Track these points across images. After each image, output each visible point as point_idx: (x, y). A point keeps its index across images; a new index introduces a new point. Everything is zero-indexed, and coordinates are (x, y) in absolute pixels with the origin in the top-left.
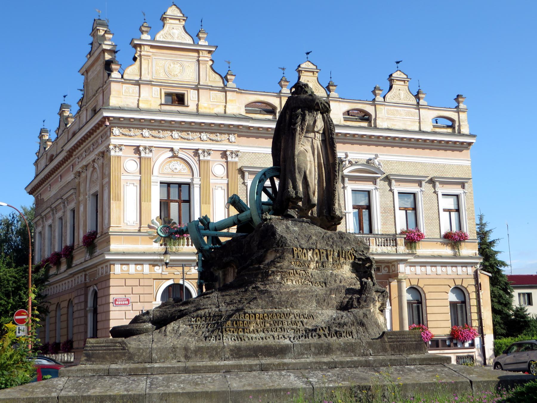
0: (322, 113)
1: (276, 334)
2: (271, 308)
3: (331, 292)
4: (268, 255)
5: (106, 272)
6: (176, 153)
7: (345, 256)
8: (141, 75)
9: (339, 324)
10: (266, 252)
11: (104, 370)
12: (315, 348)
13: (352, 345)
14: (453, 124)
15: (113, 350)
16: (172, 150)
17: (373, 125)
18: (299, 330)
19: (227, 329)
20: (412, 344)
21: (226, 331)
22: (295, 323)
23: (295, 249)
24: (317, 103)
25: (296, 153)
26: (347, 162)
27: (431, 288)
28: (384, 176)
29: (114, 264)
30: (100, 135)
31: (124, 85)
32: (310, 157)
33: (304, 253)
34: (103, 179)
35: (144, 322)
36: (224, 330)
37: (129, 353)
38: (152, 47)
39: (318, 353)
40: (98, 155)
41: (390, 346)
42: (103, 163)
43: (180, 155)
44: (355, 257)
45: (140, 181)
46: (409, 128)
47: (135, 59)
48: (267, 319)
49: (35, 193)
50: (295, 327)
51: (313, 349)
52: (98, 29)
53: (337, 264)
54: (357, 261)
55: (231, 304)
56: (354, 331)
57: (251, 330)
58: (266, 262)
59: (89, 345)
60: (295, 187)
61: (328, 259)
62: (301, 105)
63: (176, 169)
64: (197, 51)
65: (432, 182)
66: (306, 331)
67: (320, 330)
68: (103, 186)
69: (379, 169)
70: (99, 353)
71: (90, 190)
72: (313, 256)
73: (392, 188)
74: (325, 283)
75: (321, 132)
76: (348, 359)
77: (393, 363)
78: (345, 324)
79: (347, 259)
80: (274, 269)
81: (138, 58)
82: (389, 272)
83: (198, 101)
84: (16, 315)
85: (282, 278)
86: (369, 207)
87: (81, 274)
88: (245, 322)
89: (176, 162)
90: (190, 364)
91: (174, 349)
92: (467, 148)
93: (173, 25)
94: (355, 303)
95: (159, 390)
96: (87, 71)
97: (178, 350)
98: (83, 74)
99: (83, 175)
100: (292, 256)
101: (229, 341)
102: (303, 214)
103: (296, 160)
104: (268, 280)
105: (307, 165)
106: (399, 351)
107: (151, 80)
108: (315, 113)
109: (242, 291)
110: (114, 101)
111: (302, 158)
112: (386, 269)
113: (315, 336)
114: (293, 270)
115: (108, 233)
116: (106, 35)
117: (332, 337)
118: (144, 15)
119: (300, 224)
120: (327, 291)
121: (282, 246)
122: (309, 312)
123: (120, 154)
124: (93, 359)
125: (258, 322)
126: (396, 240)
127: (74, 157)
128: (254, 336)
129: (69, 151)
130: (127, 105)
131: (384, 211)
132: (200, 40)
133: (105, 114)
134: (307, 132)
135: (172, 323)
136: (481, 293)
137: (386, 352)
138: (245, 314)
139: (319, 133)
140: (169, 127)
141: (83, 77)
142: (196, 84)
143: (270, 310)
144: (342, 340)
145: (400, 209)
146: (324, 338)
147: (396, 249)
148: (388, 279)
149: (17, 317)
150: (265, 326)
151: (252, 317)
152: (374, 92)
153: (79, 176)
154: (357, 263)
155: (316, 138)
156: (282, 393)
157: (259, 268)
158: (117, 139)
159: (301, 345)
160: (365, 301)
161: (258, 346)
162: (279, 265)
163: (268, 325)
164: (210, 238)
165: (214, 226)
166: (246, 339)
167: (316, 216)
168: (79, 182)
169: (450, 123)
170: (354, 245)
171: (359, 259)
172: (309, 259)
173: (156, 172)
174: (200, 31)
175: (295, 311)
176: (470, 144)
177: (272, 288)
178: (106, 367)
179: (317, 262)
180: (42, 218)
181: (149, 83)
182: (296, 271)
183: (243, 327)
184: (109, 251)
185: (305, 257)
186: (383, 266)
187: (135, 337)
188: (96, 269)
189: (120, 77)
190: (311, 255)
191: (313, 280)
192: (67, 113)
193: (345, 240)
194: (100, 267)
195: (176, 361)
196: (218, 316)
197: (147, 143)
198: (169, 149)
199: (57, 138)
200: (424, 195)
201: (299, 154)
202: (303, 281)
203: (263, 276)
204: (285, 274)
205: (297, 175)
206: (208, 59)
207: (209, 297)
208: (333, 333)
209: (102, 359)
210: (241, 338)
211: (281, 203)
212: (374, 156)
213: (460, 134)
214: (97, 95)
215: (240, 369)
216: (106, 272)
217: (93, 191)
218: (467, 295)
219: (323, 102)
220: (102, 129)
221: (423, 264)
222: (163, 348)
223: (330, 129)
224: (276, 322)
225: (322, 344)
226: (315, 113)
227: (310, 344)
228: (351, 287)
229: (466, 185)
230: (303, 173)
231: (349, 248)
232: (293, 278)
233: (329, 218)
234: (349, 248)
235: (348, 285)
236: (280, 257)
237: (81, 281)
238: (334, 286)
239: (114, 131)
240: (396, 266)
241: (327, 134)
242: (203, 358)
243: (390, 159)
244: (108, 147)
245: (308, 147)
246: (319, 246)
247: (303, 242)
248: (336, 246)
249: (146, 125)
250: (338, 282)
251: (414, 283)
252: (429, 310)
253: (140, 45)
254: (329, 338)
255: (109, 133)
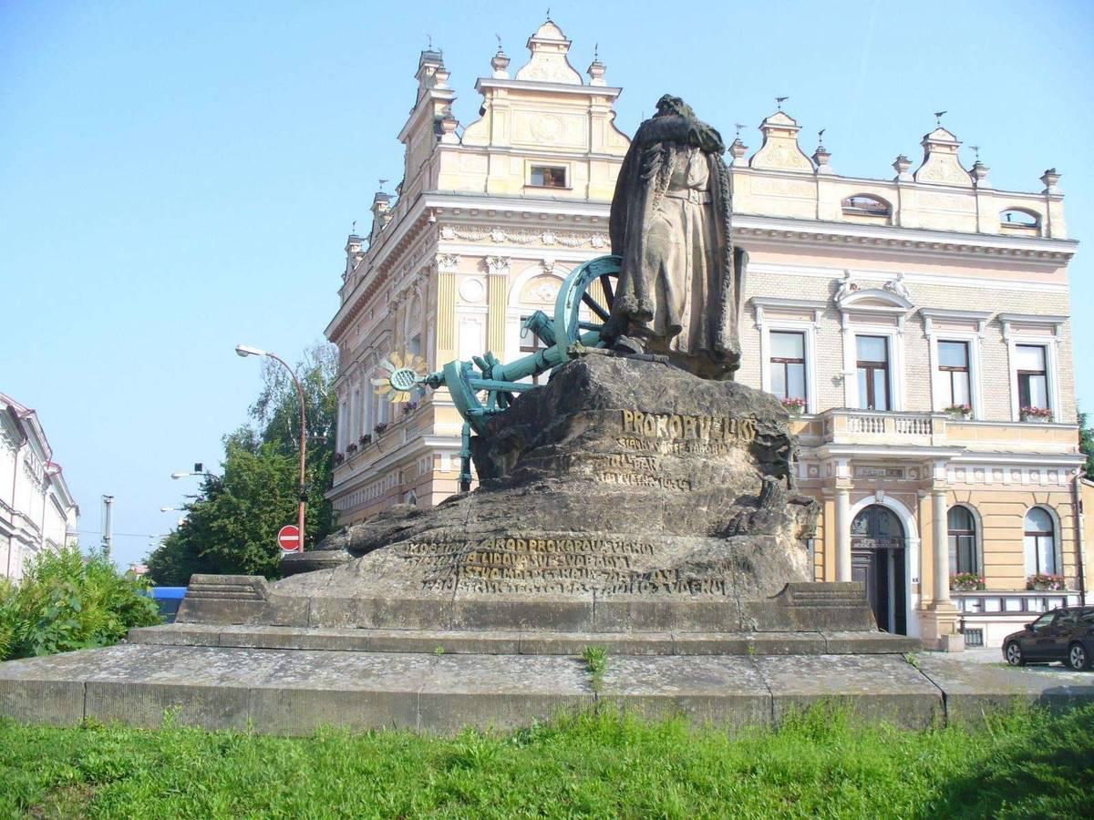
0: (706, 153)
1: (568, 581)
2: (563, 530)
3: (698, 500)
4: (574, 424)
5: (428, 469)
6: (549, 268)
7: (736, 430)
8: (491, 138)
9: (698, 565)
10: (570, 418)
11: (211, 635)
12: (639, 612)
13: (716, 607)
14: (1037, 222)
15: (239, 598)
16: (542, 262)
17: (894, 223)
18: (618, 574)
19: (468, 568)
20: (842, 611)
21: (465, 571)
22: (612, 561)
23: (627, 412)
24: (693, 131)
25: (647, 225)
26: (848, 286)
27: (993, 508)
28: (914, 310)
29: (440, 457)
30: (423, 240)
31: (463, 155)
32: (676, 235)
33: (649, 422)
34: (427, 313)
35: (336, 549)
36: (461, 569)
37: (268, 606)
38: (511, 91)
39: (644, 624)
40: (420, 273)
41: (798, 613)
42: (428, 287)
43: (555, 272)
44: (757, 431)
45: (487, 314)
46: (959, 229)
47: (482, 112)
48: (553, 550)
49: (339, 339)
50: (610, 568)
51: (634, 615)
52: (426, 67)
53: (718, 443)
54: (760, 441)
55: (488, 519)
56: (729, 581)
57: (517, 572)
58: (570, 438)
59: (196, 586)
60: (638, 293)
61: (699, 435)
62: (667, 136)
63: (549, 295)
64: (589, 97)
65: (999, 322)
66: (631, 577)
67: (656, 575)
68: (427, 323)
69: (903, 298)
70: (212, 602)
71: (409, 332)
72: (668, 429)
73: (927, 332)
74: (689, 483)
75: (704, 187)
76: (703, 638)
77: (795, 649)
78: (710, 565)
79: (740, 436)
80: (581, 452)
81: (488, 112)
82: (918, 479)
83: (589, 180)
84: (282, 535)
85: (595, 471)
86: (885, 366)
87: (393, 472)
88: (505, 555)
89: (548, 284)
90: (379, 633)
91: (353, 603)
92: (1063, 263)
93: (546, 54)
94: (745, 524)
95: (289, 683)
96: (410, 137)
97: (361, 605)
98: (403, 142)
99: (401, 307)
100: (620, 428)
101: (468, 592)
102: (657, 344)
103: (644, 241)
104: (568, 474)
105: (667, 250)
106: (816, 625)
107: (509, 146)
108: (690, 151)
109: (517, 496)
110: (445, 182)
111: (656, 236)
112: (913, 473)
113: (646, 587)
114: (620, 454)
115: (431, 402)
116: (438, 76)
117: (680, 591)
118: (499, 39)
119: (645, 364)
120: (689, 499)
121: (600, 408)
122: (646, 539)
123: (453, 269)
124: (200, 614)
125: (535, 557)
126: (930, 422)
127: (390, 278)
128: (523, 583)
129: (381, 268)
130: (468, 188)
131: (913, 372)
132: (593, 78)
133: (429, 204)
134: (673, 186)
135: (373, 552)
136: (1081, 519)
137: (787, 625)
138: (506, 539)
139: (699, 191)
140: (538, 224)
141: (405, 145)
142: (586, 151)
143: (560, 533)
144: (698, 598)
145: (940, 370)
146: (665, 592)
147: (931, 439)
148: (916, 491)
149: (283, 538)
150: (547, 564)
151: (521, 544)
152: (896, 165)
153: (396, 309)
154: (761, 445)
155: (691, 199)
156: (528, 704)
157: (553, 451)
158: (450, 244)
159: (611, 605)
160: (765, 521)
161: (522, 603)
162: (591, 443)
163: (556, 563)
164: (494, 394)
165: (501, 371)
166: (505, 590)
167: (686, 351)
168: (396, 319)
169: (1032, 220)
170: (757, 409)
171: (765, 437)
172: (659, 434)
173: (513, 302)
174: (593, 64)
175: (614, 536)
176: (1067, 256)
177: (571, 490)
178: (213, 629)
179: (675, 441)
180: (347, 380)
181: (506, 151)
182: (626, 458)
183: (500, 565)
184: (433, 433)
185: (650, 429)
186: (908, 468)
187: (300, 576)
188: (414, 463)
189: (458, 141)
190: (664, 427)
191: (661, 475)
192: (382, 209)
193: (737, 398)
194: (419, 460)
195: (354, 625)
196: (460, 541)
197: (500, 252)
198: (539, 262)
199: (370, 248)
200: (984, 344)
201: (652, 229)
202: (639, 477)
203: (558, 465)
204: (600, 460)
205: (645, 271)
206: (607, 110)
207: (457, 505)
208: (685, 582)
209: (218, 615)
210: (494, 587)
211: (620, 327)
212: (895, 276)
213: (1049, 238)
214: (422, 173)
215: (475, 649)
216: (428, 469)
217: (414, 333)
218: (1056, 521)
219: (704, 128)
220: (424, 230)
221: (979, 467)
222: (333, 599)
223: (721, 183)
224: (575, 561)
225: (654, 605)
226: (690, 151)
227: (629, 604)
228: (746, 492)
229: (1059, 328)
230: (658, 266)
231: (744, 414)
232: (617, 471)
233: (713, 359)
234: (744, 414)
235: (738, 488)
236: (594, 429)
237: (395, 483)
238: (707, 487)
239: (444, 232)
240: (930, 469)
241: (714, 190)
242: (409, 624)
243: (926, 284)
244: (433, 259)
245: (677, 220)
246: (680, 409)
247: (646, 400)
248: (718, 410)
249: (499, 221)
250: (717, 481)
251: (962, 498)
252: (988, 546)
253: (491, 89)
254: (675, 593)
255: (436, 236)
